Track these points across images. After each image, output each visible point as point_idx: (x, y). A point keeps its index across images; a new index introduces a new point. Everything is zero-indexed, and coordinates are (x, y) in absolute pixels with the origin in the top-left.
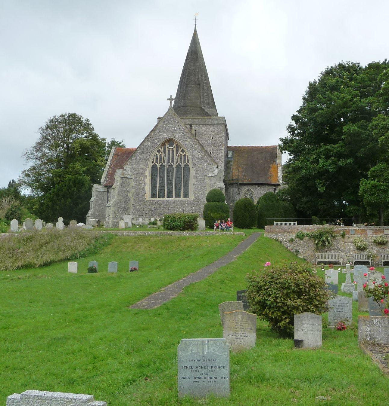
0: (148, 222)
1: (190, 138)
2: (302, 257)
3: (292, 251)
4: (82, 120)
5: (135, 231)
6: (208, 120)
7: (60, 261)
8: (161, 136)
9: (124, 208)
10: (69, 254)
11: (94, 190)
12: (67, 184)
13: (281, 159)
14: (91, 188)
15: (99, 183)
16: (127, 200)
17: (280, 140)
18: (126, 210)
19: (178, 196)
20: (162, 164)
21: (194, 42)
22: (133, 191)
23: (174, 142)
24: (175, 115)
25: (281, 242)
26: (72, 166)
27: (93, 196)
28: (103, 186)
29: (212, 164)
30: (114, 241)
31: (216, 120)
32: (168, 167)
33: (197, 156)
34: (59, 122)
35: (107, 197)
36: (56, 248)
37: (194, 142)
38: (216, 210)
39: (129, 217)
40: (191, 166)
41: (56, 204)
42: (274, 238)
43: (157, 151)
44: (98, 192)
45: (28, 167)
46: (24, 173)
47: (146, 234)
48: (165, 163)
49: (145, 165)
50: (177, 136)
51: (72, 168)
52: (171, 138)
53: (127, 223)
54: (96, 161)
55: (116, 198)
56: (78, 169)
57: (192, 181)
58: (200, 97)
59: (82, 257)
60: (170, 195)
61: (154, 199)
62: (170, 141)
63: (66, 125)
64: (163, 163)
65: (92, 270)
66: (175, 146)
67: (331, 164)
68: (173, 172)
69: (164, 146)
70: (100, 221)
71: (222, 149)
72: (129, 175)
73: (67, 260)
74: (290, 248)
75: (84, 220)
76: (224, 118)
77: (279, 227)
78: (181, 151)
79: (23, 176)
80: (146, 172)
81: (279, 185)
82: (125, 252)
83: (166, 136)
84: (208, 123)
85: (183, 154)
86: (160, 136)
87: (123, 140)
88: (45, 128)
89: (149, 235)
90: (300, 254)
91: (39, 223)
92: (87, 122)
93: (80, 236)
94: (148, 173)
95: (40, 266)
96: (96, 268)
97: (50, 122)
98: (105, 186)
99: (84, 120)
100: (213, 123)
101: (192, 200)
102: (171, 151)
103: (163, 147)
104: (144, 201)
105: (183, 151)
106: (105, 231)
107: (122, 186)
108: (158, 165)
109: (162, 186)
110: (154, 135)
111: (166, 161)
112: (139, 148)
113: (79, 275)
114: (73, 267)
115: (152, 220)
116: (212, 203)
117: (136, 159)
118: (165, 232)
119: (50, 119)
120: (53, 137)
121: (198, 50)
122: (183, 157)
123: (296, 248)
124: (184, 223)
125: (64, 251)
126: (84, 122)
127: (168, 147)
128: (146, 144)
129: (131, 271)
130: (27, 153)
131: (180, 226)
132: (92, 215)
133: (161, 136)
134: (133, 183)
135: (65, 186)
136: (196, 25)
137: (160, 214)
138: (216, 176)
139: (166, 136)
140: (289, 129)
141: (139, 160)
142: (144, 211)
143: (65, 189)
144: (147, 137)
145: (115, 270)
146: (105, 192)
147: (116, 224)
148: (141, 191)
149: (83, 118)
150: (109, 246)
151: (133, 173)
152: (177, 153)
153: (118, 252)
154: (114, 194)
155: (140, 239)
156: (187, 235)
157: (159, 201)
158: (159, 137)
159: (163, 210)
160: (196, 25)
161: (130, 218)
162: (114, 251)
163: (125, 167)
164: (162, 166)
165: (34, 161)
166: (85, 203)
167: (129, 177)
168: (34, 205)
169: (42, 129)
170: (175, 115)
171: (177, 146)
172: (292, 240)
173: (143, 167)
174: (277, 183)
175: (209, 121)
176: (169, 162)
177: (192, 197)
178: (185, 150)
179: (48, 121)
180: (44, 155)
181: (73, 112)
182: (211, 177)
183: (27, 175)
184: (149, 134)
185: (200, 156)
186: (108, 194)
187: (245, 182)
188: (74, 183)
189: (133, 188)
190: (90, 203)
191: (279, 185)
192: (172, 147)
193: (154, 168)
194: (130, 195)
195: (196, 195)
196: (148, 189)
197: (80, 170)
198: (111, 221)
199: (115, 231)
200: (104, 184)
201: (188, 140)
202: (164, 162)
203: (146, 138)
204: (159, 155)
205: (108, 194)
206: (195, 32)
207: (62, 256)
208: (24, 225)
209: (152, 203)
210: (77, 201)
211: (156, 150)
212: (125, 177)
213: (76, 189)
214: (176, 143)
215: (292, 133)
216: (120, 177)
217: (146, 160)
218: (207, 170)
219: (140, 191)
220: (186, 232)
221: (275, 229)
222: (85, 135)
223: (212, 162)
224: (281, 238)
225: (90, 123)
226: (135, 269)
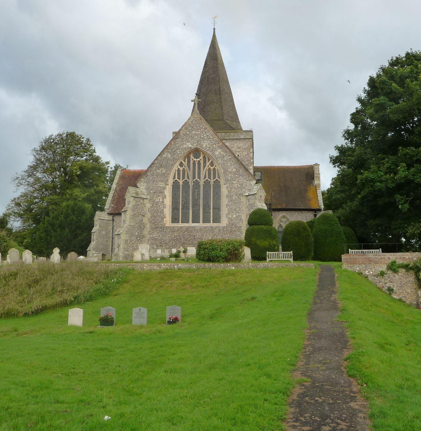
0: (168, 254)
1: (220, 147)
2: (398, 298)
3: (384, 290)
4: (82, 140)
5: (160, 264)
6: (232, 134)
7: (54, 307)
8: (184, 146)
9: (137, 237)
10: (68, 296)
11: (96, 218)
12: (64, 211)
13: (319, 179)
14: (93, 216)
15: (102, 209)
16: (141, 227)
17: (335, 149)
18: (140, 238)
19: (206, 220)
20: (186, 180)
21: (213, 47)
22: (149, 215)
23: (200, 153)
24: (201, 120)
25: (366, 277)
26: (70, 192)
27: (95, 226)
28: (107, 213)
29: (249, 180)
30: (131, 277)
31: (242, 134)
32: (193, 184)
33: (230, 170)
34: (56, 143)
35: (112, 227)
36: (49, 288)
37: (226, 152)
38: (260, 236)
39: (146, 247)
40: (222, 181)
41: (51, 235)
42: (357, 271)
43: (179, 165)
44: (101, 221)
45: (18, 194)
46: (14, 202)
47: (176, 267)
48: (189, 179)
49: (164, 182)
50: (205, 145)
51: (69, 197)
52: (197, 148)
53: (144, 254)
54: (97, 186)
55: (128, 222)
56: (76, 196)
57: (224, 201)
58: (222, 109)
59: (87, 301)
60: (196, 220)
61: (175, 225)
62: (196, 152)
63: (64, 147)
64: (187, 179)
65: (107, 321)
66: (201, 157)
67: (416, 173)
68: (199, 191)
69: (188, 158)
70: (105, 255)
71: (250, 168)
72: (144, 194)
73: (67, 304)
74: (380, 285)
75: (84, 253)
76: (251, 131)
77: (361, 256)
78: (210, 164)
79: (13, 205)
80: (165, 191)
81: (320, 210)
82: (149, 292)
83: (190, 146)
84: (233, 138)
85: (212, 168)
86: (182, 145)
87: (128, 166)
88: (39, 150)
89: (179, 269)
90: (395, 293)
91: (28, 255)
92: (87, 142)
93: (83, 272)
94: (168, 192)
95: (26, 315)
96: (112, 318)
97: (45, 143)
98: (109, 214)
99: (84, 140)
100: (239, 138)
101: (225, 226)
102: (197, 165)
103: (186, 159)
104: (163, 228)
105: (212, 164)
106: (117, 264)
107: (135, 208)
108: (181, 182)
109: (185, 207)
110: (175, 144)
111: (191, 177)
112: (156, 161)
113: (87, 330)
114: (76, 316)
115: (174, 251)
116: (255, 227)
117: (153, 175)
118: (202, 264)
119: (45, 138)
120: (48, 160)
121: (218, 56)
122: (212, 172)
123: (388, 285)
124: (227, 251)
125: (62, 292)
126: (84, 142)
127: (193, 160)
128: (164, 156)
129: (170, 323)
130: (17, 178)
131: (223, 257)
132: (94, 249)
133: (184, 146)
134: (148, 205)
135: (62, 214)
136: (214, 29)
137: (184, 243)
138: (256, 194)
139: (189, 145)
140: (346, 135)
141: (157, 175)
142: (163, 240)
143: (62, 218)
144: (166, 147)
145: (144, 321)
146: (110, 221)
147: (127, 256)
148: (159, 214)
149: (83, 138)
150: (125, 285)
151: (149, 192)
152: (204, 166)
153: (139, 292)
154: (127, 218)
155: (167, 275)
156: (233, 268)
157: (182, 227)
158: (182, 147)
159: (187, 238)
160: (214, 29)
161: (148, 248)
162: (133, 292)
163: (138, 185)
164: (186, 183)
165: (26, 187)
166: (85, 234)
167: (144, 197)
168: (24, 238)
169: (35, 150)
170: (201, 120)
171: (204, 157)
172: (382, 274)
173: (162, 184)
174: (318, 208)
175: (235, 135)
176: (194, 178)
177: (224, 222)
178: (215, 163)
179: (43, 141)
180: (38, 180)
181: (72, 131)
182: (249, 195)
183: (18, 205)
184: (169, 144)
185: (234, 170)
186: (113, 223)
187: (279, 207)
188: (73, 210)
189: (149, 211)
190: (92, 233)
191: (320, 210)
192: (198, 160)
193: (176, 185)
194: (145, 220)
195: (230, 219)
196: (168, 212)
197: (79, 197)
198: (121, 254)
199: (132, 264)
200: (109, 212)
201: (218, 150)
202: (188, 178)
203: (165, 149)
204: (181, 170)
205: (113, 223)
206: (214, 36)
207: (57, 299)
208: (8, 259)
209: (173, 230)
210: (76, 232)
211: (178, 163)
212: (139, 197)
213: (74, 218)
214: (203, 154)
215: (349, 140)
216: (132, 197)
217: (165, 177)
218: (243, 187)
219: (157, 214)
220: (231, 264)
221: (356, 258)
222: (85, 158)
223: (249, 177)
224: (367, 271)
225: (91, 143)
226: (175, 320)
